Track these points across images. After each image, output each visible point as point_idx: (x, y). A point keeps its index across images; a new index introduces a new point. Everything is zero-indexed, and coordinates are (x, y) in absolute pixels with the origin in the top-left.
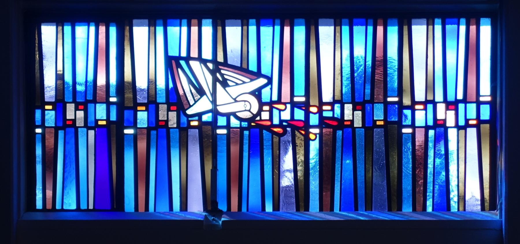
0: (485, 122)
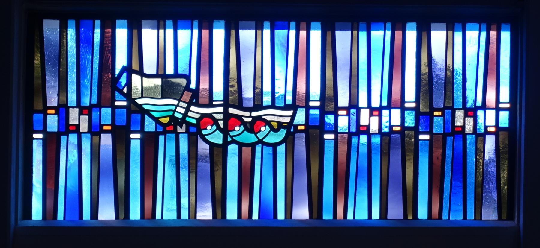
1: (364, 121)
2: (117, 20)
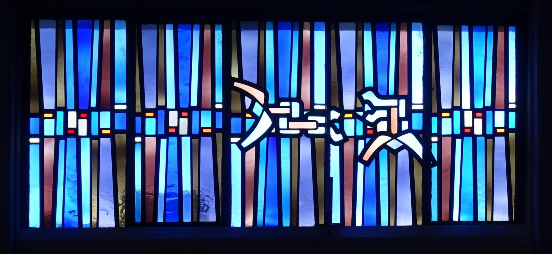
0: (512, 130)
2: (109, 21)
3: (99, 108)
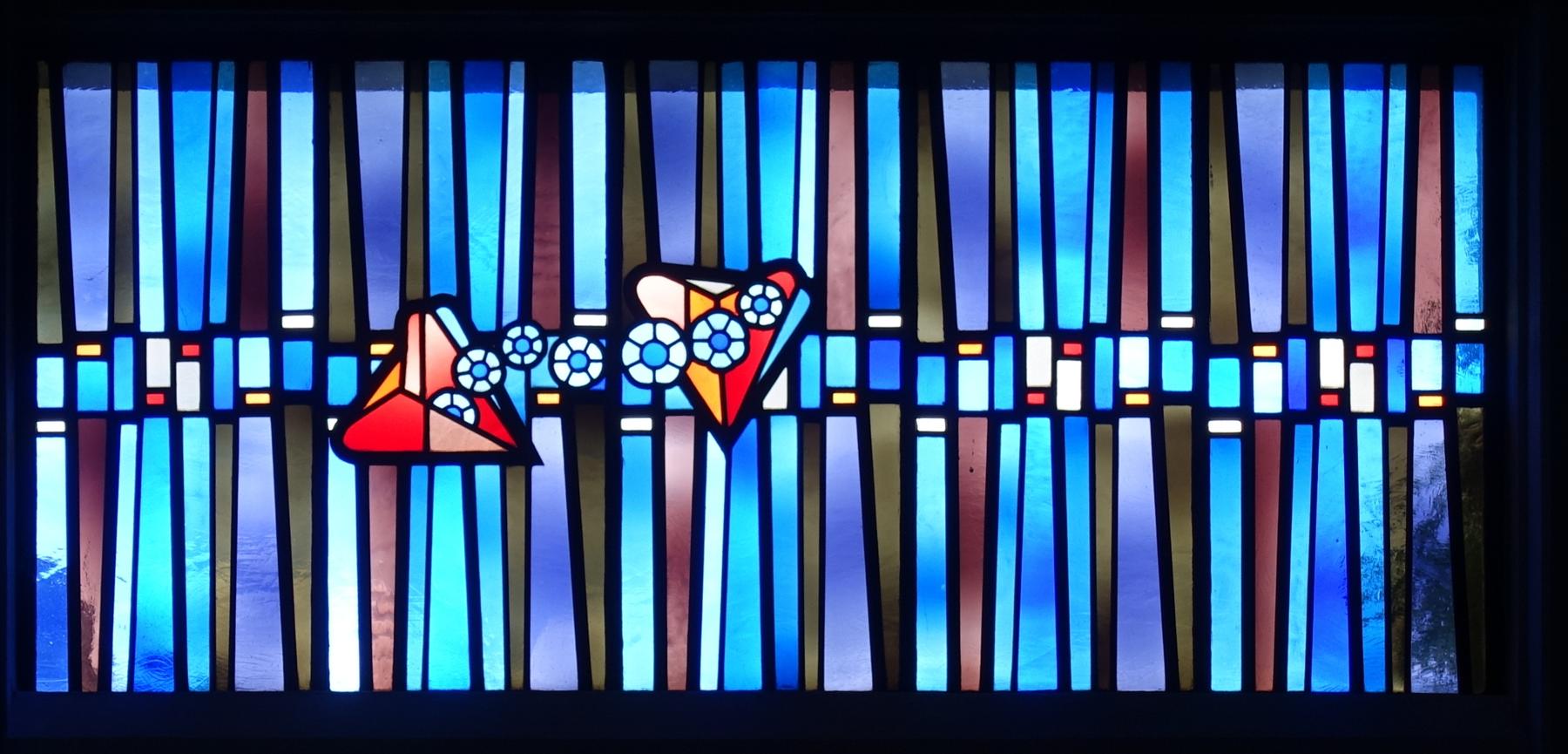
1: (157, 376)
2: (1236, 64)
3: (235, 329)
